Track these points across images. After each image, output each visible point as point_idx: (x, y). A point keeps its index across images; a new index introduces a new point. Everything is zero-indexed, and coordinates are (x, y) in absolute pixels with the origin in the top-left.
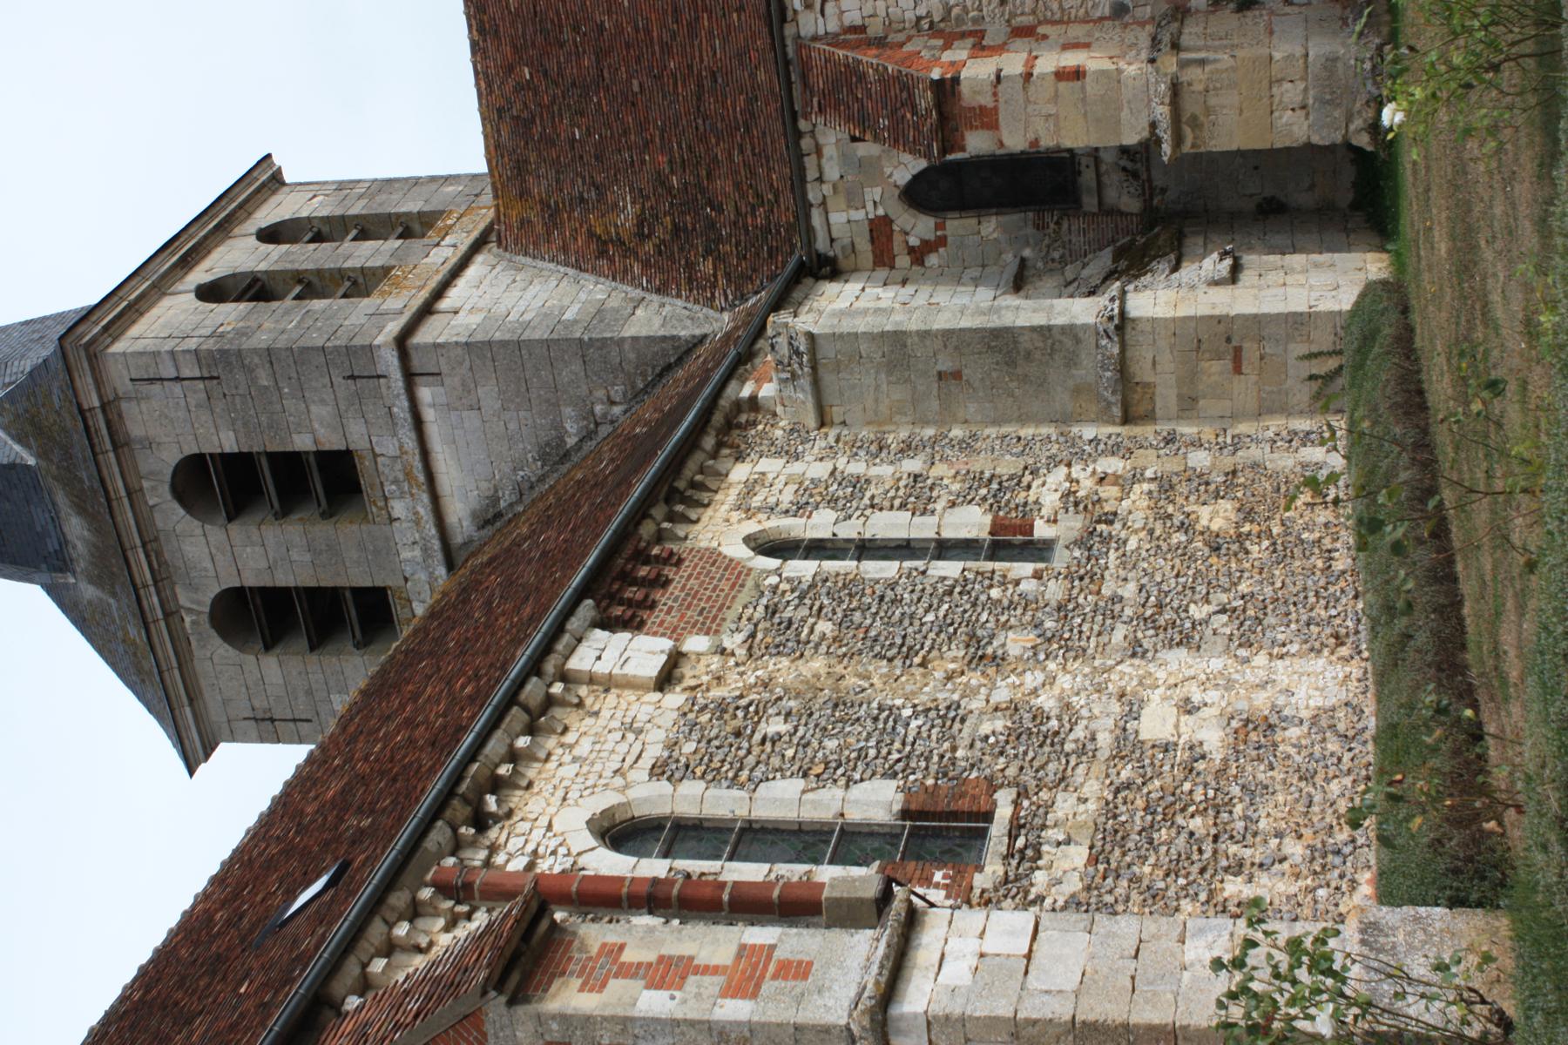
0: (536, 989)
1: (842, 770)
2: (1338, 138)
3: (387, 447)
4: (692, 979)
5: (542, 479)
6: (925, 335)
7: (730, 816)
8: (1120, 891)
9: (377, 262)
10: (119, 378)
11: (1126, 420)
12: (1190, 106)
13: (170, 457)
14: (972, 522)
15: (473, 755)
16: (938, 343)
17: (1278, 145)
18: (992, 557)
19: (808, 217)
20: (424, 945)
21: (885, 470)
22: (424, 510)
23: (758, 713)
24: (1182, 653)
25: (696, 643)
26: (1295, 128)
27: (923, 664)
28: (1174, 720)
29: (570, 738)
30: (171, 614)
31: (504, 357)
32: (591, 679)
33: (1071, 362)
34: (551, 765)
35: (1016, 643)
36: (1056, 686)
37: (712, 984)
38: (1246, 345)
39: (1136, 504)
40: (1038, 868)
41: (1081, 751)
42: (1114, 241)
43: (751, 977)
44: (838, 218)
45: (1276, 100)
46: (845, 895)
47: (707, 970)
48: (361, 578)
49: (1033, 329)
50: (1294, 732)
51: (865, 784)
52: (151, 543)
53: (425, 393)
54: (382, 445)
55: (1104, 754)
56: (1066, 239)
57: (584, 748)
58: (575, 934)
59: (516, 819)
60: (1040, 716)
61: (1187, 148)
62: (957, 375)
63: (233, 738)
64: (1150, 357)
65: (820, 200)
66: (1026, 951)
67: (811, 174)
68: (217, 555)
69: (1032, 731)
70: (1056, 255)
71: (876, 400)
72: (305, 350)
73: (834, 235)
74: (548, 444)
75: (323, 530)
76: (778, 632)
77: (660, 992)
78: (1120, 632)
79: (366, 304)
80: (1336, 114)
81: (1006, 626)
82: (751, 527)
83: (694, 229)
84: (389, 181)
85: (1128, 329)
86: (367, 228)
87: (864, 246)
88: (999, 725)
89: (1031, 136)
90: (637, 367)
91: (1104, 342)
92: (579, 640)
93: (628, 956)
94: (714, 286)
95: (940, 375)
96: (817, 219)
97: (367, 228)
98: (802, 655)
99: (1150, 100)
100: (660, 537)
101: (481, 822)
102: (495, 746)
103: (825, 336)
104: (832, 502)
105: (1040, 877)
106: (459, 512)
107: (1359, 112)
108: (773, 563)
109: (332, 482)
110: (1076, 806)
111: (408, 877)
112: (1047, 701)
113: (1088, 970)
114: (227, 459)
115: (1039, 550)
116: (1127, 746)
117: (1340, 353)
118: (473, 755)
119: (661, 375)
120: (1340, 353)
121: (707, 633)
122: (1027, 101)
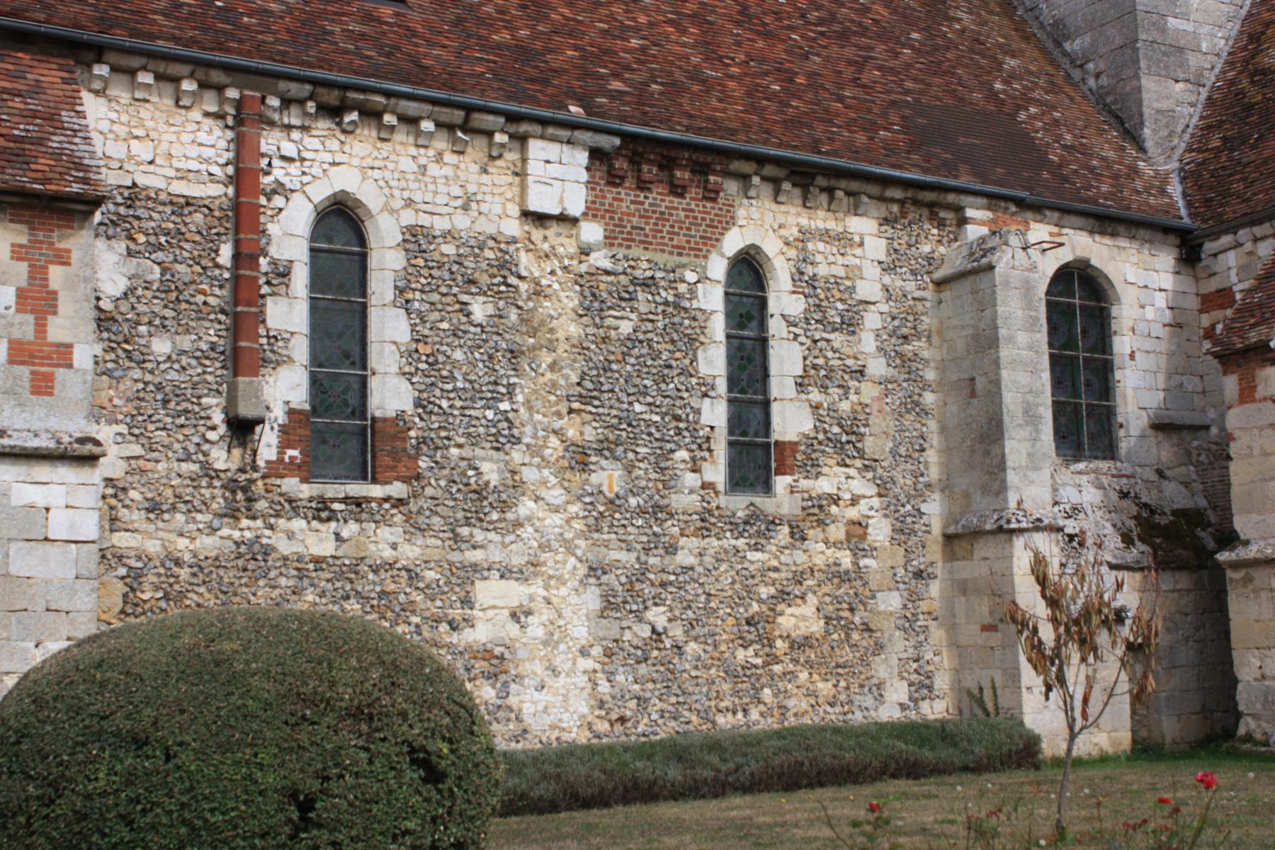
0: (11, 214)
2: (1241, 708)
4: (31, 318)
5: (1042, 26)
6: (996, 363)
7: (369, 292)
8: (283, 581)
11: (949, 538)
14: (790, 421)
16: (992, 376)
17: (1234, 654)
19: (1226, 232)
20: (181, 103)
21: (868, 343)
25: (592, 232)
26: (1246, 670)
27: (571, 411)
28: (500, 603)
29: (450, 158)
33: (985, 490)
34: (413, 151)
36: (548, 509)
38: (999, 635)
39: (818, 552)
40: (309, 522)
41: (456, 538)
42: (1214, 508)
43: (32, 357)
44: (1231, 259)
45: (1267, 652)
46: (240, 393)
47: (41, 328)
49: (1003, 455)
51: (410, 387)
56: (1216, 465)
57: (434, 170)
58: (82, 228)
59: (343, 138)
61: (1230, 574)
62: (973, 394)
64: (989, 555)
65: (1241, 241)
66: (51, 537)
67: (1258, 231)
70: (1203, 458)
71: (955, 327)
73: (1220, 257)
74: (1065, 26)
77: (14, 299)
80: (1258, 706)
81: (629, 468)
82: (771, 247)
83: (1246, 124)
85: (1005, 536)
87: (1212, 285)
89: (1236, 433)
90: (1120, 95)
91: (995, 517)
92: (569, 142)
94: (1199, 151)
95: (973, 380)
96: (1226, 240)
98: (581, 316)
99: (1265, 539)
103: (993, 280)
105: (298, 524)
107: (1259, 726)
111: (240, 77)
112: (526, 507)
113: (31, 581)
117: (997, 714)
118: (388, 94)
119: (1117, 117)
120: (997, 714)
121: (606, 237)
122: (1261, 429)
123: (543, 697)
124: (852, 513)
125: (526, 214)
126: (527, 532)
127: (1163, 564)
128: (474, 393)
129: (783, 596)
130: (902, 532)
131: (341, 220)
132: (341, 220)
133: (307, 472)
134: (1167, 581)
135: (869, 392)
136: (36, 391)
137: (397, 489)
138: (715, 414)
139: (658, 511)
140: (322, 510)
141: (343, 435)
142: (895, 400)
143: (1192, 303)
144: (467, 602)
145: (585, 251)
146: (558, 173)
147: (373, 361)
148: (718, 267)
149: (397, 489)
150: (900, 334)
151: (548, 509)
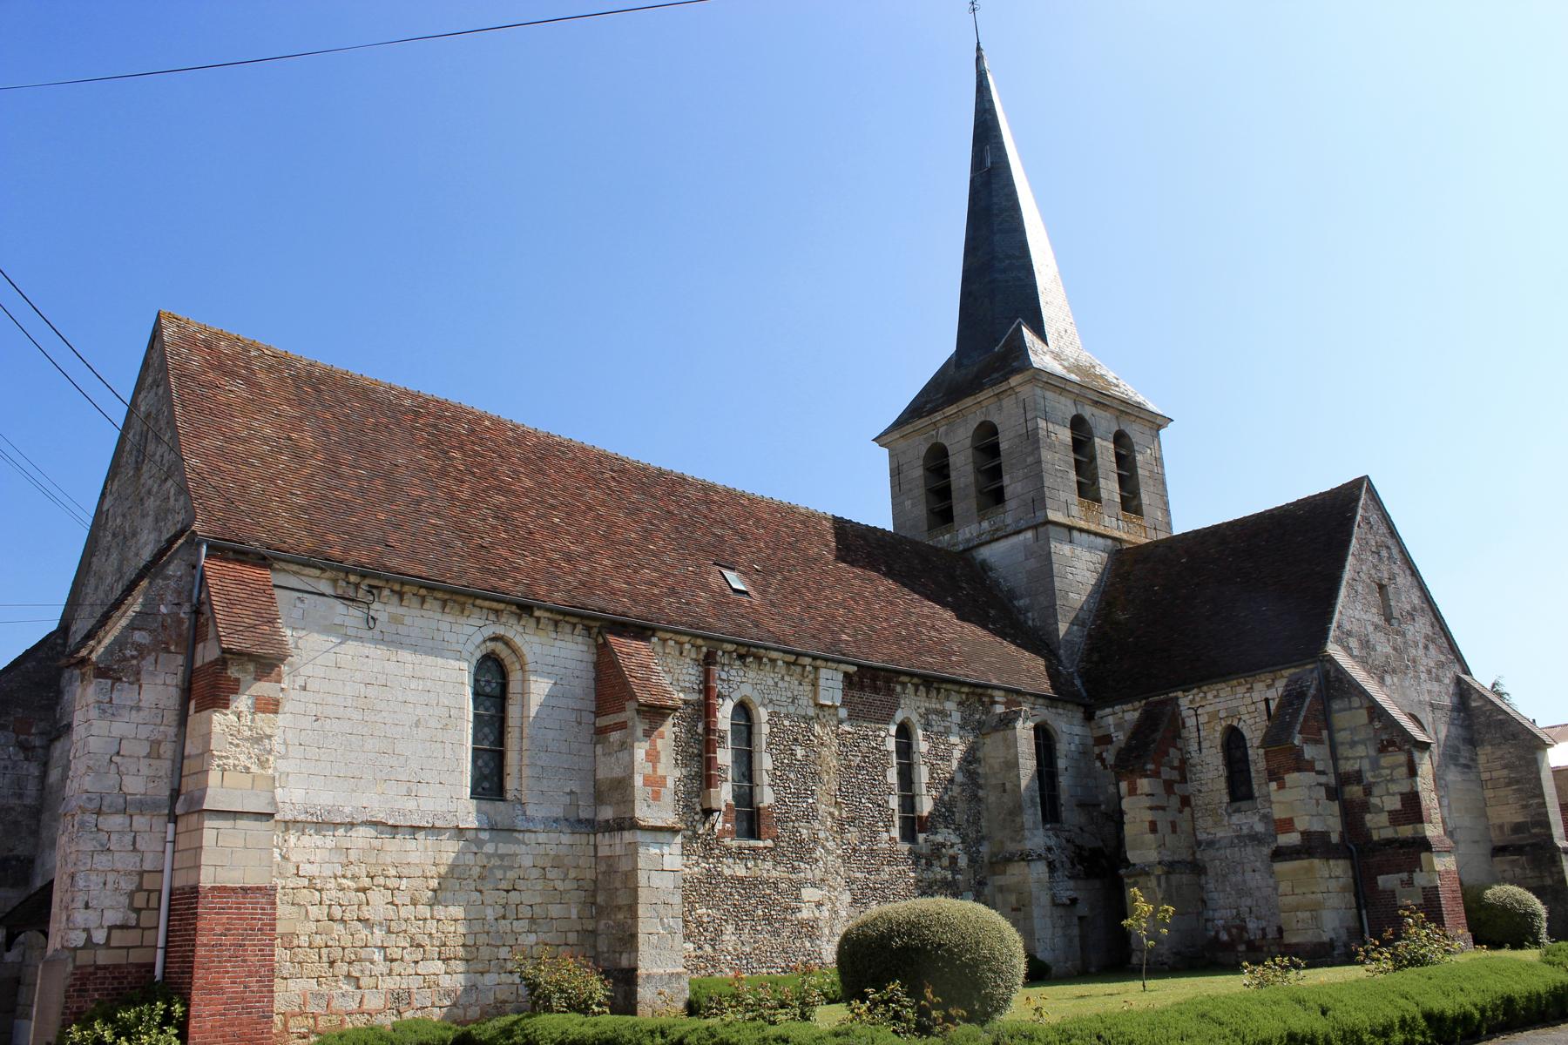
1: (778, 779)
9: (1104, 494)
15: (767, 649)
18: (904, 820)
23: (807, 745)
25: (843, 713)
31: (1044, 570)
32: (817, 679)
36: (829, 855)
37: (649, 770)
44: (1111, 720)
47: (654, 768)
48: (956, 511)
53: (1029, 534)
55: (793, 876)
57: (781, 684)
63: (891, 456)
72: (1042, 478)
75: (972, 491)
78: (858, 875)
79: (1074, 497)
82: (915, 718)
84: (1164, 483)
87: (1101, 733)
96: (1108, 710)
100: (904, 684)
101: (741, 657)
102: (774, 655)
106: (985, 553)
109: (993, 496)
114: (997, 445)
115: (909, 834)
116: (798, 886)
118: (767, 649)
124: (951, 852)
125: (817, 705)
127: (1089, 875)
134: (1097, 884)
136: (655, 799)
138: (894, 802)
140: (739, 855)
141: (750, 820)
143: (1090, 741)
144: (798, 898)
147: (757, 780)
148: (893, 729)
149: (769, 843)
151: (829, 855)
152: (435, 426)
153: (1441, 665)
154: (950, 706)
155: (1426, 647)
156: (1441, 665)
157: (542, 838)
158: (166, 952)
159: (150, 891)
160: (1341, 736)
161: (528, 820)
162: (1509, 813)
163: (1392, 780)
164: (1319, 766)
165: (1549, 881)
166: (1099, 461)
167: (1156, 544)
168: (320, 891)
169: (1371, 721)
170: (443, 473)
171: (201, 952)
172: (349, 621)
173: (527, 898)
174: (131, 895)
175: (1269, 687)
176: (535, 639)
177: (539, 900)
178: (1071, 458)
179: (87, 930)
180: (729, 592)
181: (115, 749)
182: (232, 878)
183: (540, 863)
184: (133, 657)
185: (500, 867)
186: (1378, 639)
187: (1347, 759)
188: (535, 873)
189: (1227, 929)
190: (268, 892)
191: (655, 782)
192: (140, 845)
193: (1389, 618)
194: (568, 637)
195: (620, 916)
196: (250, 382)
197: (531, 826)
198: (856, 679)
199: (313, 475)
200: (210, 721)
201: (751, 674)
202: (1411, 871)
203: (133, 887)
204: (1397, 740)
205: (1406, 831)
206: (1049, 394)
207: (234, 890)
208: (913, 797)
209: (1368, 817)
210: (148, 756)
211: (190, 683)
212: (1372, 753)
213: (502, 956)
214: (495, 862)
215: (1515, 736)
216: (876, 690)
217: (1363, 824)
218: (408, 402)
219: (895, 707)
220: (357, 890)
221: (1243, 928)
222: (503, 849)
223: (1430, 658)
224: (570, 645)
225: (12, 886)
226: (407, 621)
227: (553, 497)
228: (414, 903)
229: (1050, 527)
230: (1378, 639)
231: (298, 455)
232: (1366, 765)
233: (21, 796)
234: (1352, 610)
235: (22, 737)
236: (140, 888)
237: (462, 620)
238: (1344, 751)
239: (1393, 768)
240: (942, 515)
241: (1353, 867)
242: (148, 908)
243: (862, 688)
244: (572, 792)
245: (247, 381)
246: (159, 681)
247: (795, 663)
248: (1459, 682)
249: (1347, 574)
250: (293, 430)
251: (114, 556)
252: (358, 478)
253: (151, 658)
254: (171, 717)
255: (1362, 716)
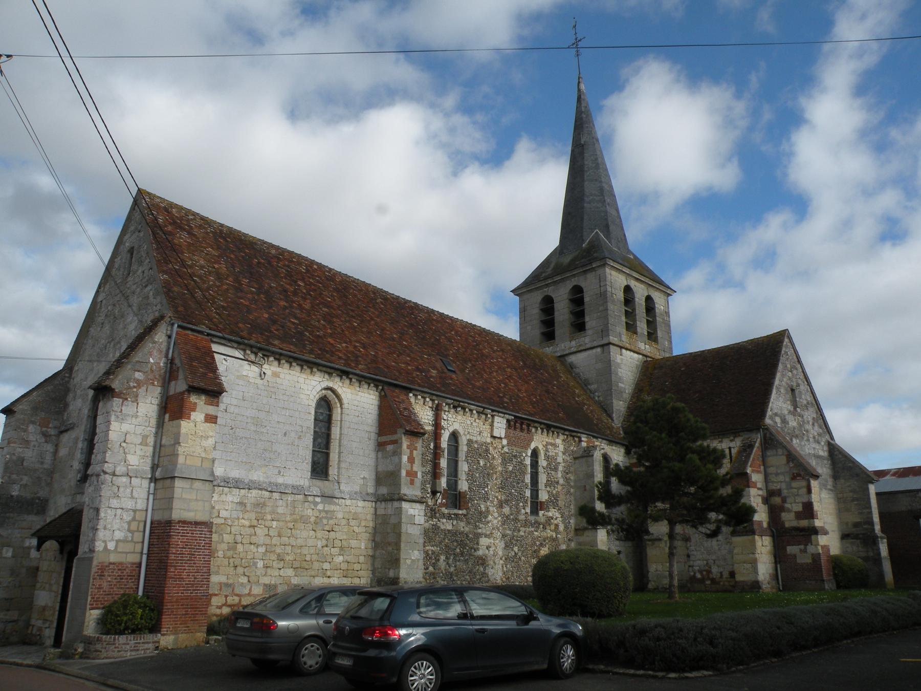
3: (587, 340)
9: (639, 330)
10: (600, 271)
11: (576, 530)
12: (657, 543)
13: (583, 285)
14: (543, 496)
21: (560, 475)
22: (573, 350)
24: (503, 546)
25: (505, 442)
30: (547, 285)
31: (607, 369)
32: (493, 422)
35: (506, 510)
36: (494, 519)
39: (549, 533)
41: (476, 526)
47: (412, 467)
48: (557, 333)
50: (482, 569)
52: (563, 280)
53: (599, 350)
54: (587, 339)
57: (474, 424)
60: (486, 517)
68: (561, 296)
69: (482, 516)
76: (506, 459)
78: (508, 532)
79: (624, 331)
81: (511, 508)
82: (540, 447)
84: (669, 326)
86: (651, 324)
88: (483, 509)
93: (415, 452)
97: (651, 324)
100: (536, 428)
101: (455, 407)
104: (549, 464)
105: (445, 520)
106: (572, 359)
108: (529, 454)
109: (579, 326)
110: (462, 526)
112: (490, 518)
115: (535, 512)
116: (478, 536)
123: (493, 571)
126: (490, 525)
127: (627, 539)
128: (479, 486)
129: (541, 545)
130: (566, 527)
131: (454, 436)
132: (454, 436)
133: (446, 506)
134: (629, 544)
135: (560, 488)
137: (464, 512)
138: (528, 493)
139: (516, 520)
140: (449, 517)
142: (565, 490)
144: (478, 544)
145: (503, 447)
146: (500, 425)
147: (459, 476)
149: (464, 512)
150: (566, 472)
152: (288, 266)
153: (820, 435)
154: (559, 441)
155: (813, 424)
156: (820, 435)
157: (348, 502)
158: (148, 556)
159: (139, 521)
160: (771, 470)
161: (341, 492)
162: (853, 518)
163: (798, 495)
164: (759, 485)
165: (871, 554)
166: (637, 312)
167: (668, 359)
168: (230, 526)
169: (788, 462)
170: (295, 293)
171: (172, 557)
172: (251, 374)
173: (339, 535)
174: (129, 523)
175: (731, 441)
176: (349, 391)
177: (345, 537)
178: (623, 308)
179: (105, 542)
180: (446, 371)
181: (122, 440)
182: (190, 516)
183: (347, 517)
184: (134, 387)
185: (326, 518)
186: (790, 418)
187: (773, 482)
188: (344, 522)
189: (701, 572)
190: (208, 525)
191: (411, 474)
192: (135, 494)
193: (795, 407)
194: (366, 391)
195: (390, 549)
196: (190, 233)
197: (343, 496)
198: (512, 423)
199: (227, 289)
200: (179, 426)
201: (459, 417)
202: (806, 545)
203: (130, 518)
204: (802, 473)
205: (804, 523)
206: (614, 273)
207: (190, 523)
208: (537, 491)
209: (783, 514)
210: (141, 444)
211: (166, 404)
212: (788, 479)
213: (324, 567)
214: (323, 514)
215: (857, 475)
216: (522, 430)
217: (780, 518)
218: (273, 252)
219: (531, 440)
220: (250, 526)
221: (709, 572)
222: (327, 508)
223: (815, 430)
224: (366, 395)
225: (36, 514)
226: (282, 376)
227: (352, 311)
228: (280, 536)
229: (611, 346)
230: (790, 418)
231: (219, 276)
232: (784, 486)
233: (42, 463)
234: (778, 403)
235: (44, 429)
236: (134, 519)
237: (311, 377)
238: (773, 478)
239: (799, 488)
240: (549, 335)
241: (774, 542)
242: (138, 531)
243: (515, 429)
244: (364, 478)
245: (189, 233)
246: (148, 401)
247: (482, 413)
248: (829, 444)
249: (777, 382)
250: (215, 263)
251: (107, 328)
252: (252, 293)
253: (144, 388)
254: (153, 422)
255: (783, 460)
